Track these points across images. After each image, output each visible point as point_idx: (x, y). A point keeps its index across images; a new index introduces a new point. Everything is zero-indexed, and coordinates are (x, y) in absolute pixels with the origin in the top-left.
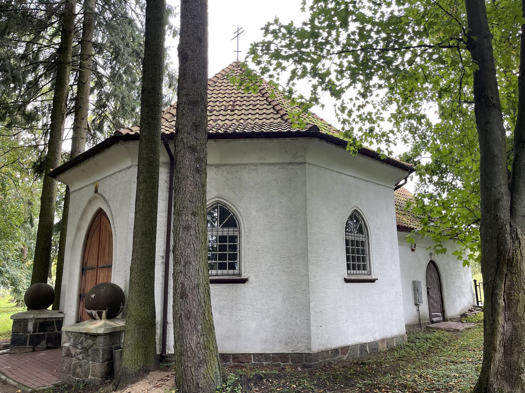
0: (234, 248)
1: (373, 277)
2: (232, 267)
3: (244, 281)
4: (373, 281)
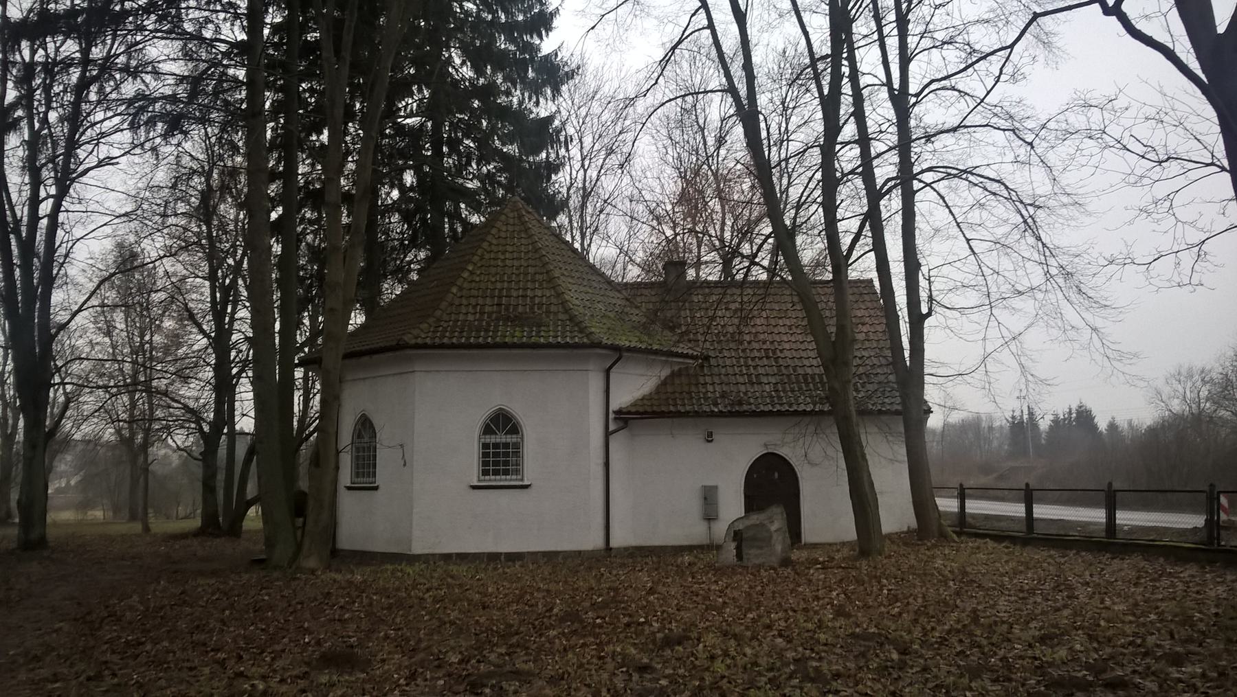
0: (485, 463)
1: (526, 483)
2: (517, 472)
3: (376, 488)
4: (527, 487)
